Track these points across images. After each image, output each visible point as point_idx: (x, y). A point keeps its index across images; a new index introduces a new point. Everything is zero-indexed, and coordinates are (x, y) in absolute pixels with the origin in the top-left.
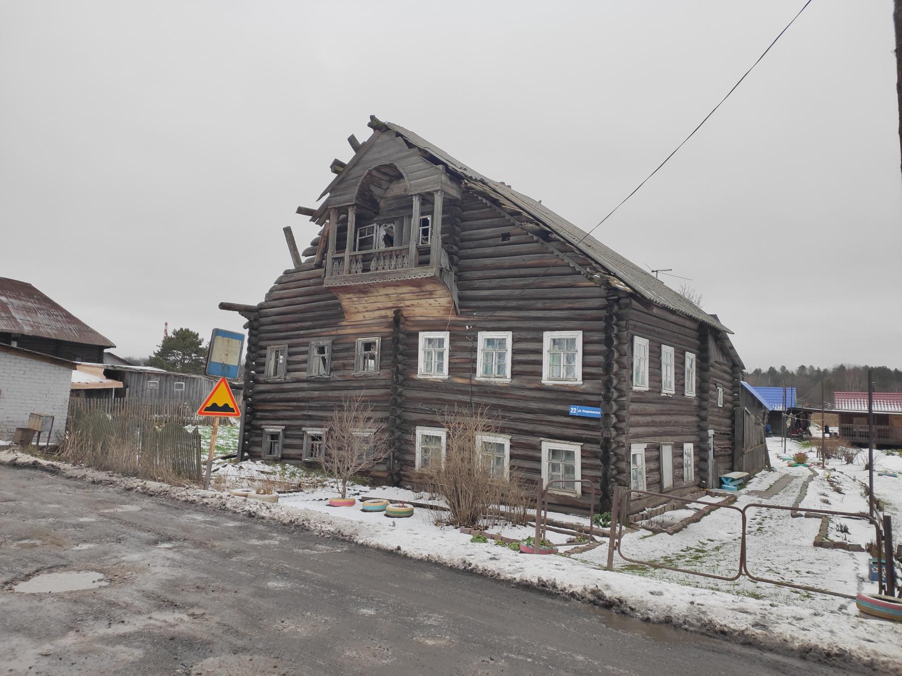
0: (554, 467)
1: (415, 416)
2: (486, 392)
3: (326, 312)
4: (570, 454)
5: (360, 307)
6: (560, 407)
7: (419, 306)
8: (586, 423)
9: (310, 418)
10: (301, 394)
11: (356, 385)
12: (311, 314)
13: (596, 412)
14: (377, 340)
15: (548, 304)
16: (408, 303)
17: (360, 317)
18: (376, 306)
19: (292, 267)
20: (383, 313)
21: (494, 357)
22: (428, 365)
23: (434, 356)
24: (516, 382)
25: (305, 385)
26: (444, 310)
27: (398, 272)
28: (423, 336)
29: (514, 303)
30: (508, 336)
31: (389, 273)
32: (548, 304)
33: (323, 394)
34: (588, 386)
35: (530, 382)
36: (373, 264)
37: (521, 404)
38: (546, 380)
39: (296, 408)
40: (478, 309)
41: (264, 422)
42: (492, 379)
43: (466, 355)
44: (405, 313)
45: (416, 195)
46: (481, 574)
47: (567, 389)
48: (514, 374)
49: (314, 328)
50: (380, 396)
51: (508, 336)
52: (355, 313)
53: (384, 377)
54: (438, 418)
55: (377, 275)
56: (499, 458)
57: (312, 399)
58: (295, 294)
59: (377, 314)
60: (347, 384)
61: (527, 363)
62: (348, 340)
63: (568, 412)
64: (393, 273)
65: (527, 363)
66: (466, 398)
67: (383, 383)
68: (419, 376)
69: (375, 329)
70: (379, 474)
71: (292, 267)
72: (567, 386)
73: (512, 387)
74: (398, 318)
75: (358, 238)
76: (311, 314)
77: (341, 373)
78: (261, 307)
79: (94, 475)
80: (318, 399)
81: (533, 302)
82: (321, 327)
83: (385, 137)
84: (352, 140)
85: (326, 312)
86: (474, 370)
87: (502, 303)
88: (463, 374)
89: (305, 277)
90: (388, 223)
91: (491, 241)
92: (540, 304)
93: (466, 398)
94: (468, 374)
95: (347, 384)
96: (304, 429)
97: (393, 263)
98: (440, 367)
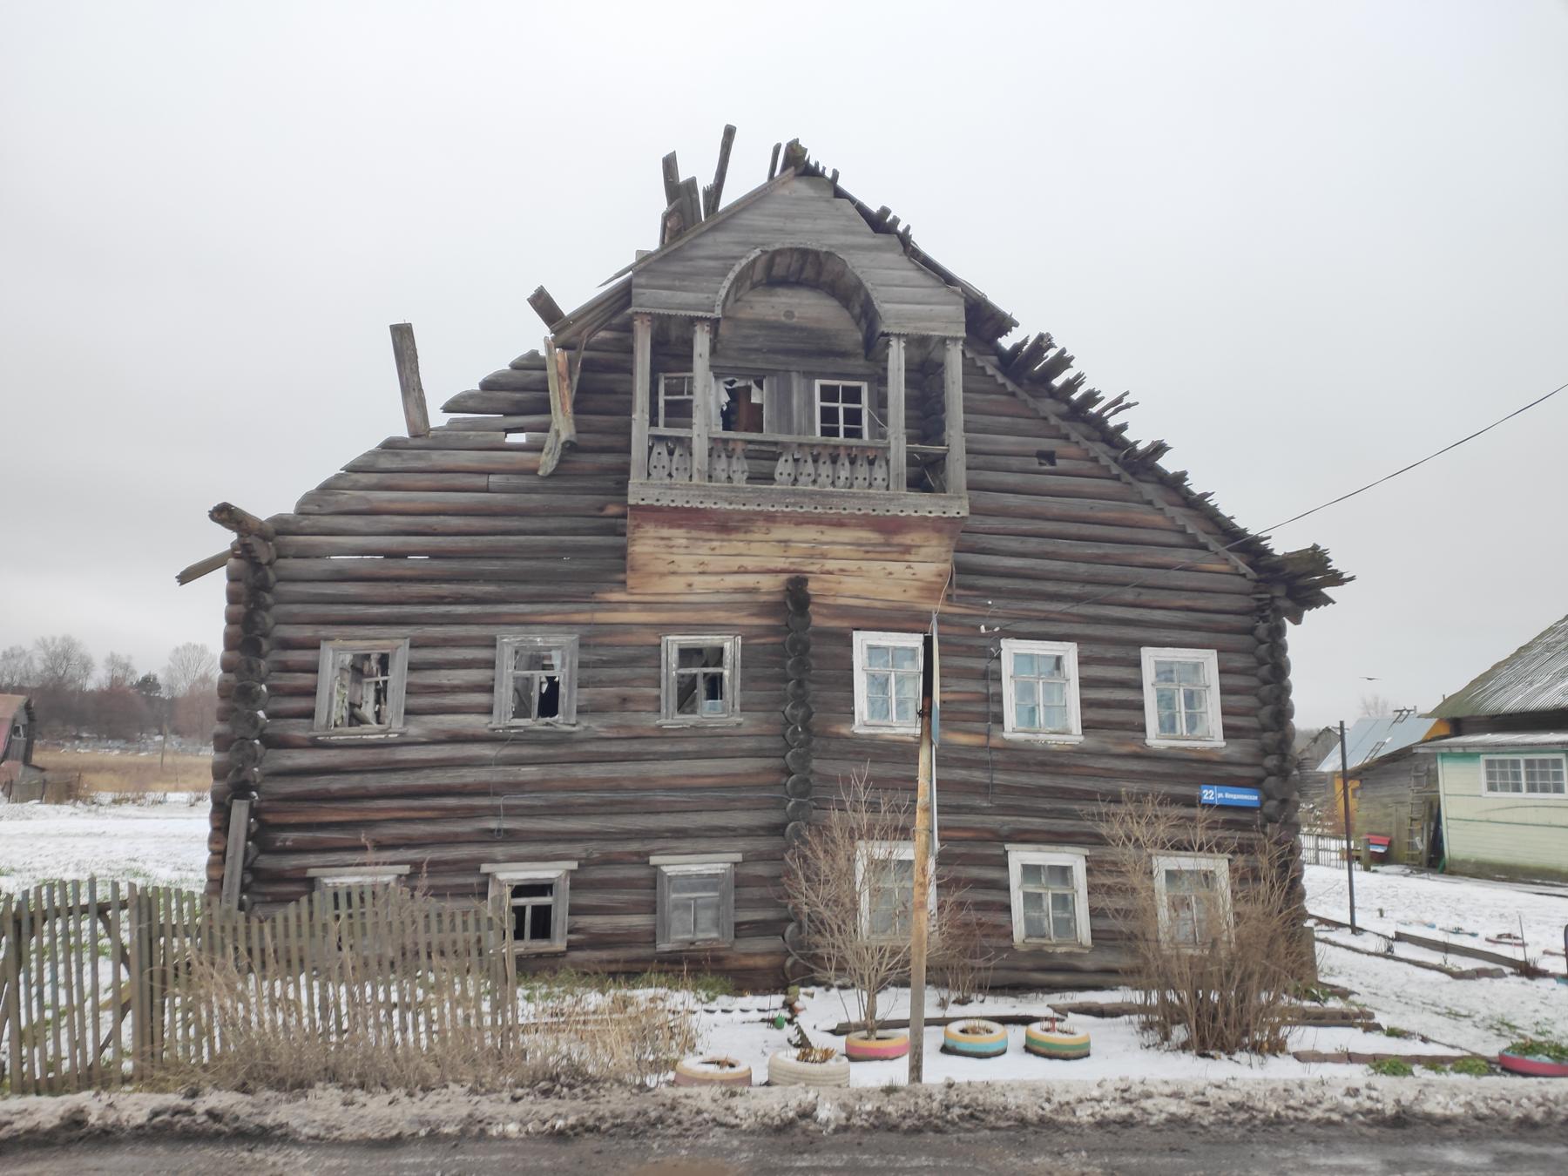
0: (1032, 900)
4: (1064, 873)
5: (685, 562)
6: (1181, 790)
7: (859, 573)
8: (1234, 818)
9: (510, 836)
10: (470, 776)
11: (666, 748)
12: (496, 565)
13: (1248, 797)
14: (731, 646)
15: (1147, 596)
16: (831, 565)
17: (676, 585)
18: (735, 563)
19: (402, 432)
20: (749, 581)
21: (1041, 693)
24: (1092, 742)
25: (487, 751)
26: (922, 589)
28: (862, 641)
29: (1075, 589)
30: (1069, 652)
32: (1147, 596)
33: (556, 772)
34: (1235, 750)
36: (783, 468)
40: (996, 593)
41: (311, 859)
42: (1041, 737)
43: (975, 686)
44: (813, 587)
45: (899, 336)
47: (1194, 755)
48: (1087, 726)
50: (748, 775)
51: (1069, 652)
52: (662, 575)
53: (752, 730)
55: (811, 495)
56: (1065, 897)
57: (517, 787)
58: (433, 506)
60: (636, 746)
61: (1113, 706)
65: (1113, 706)
66: (978, 776)
67: (749, 744)
68: (858, 728)
69: (721, 616)
70: (750, 962)
71: (402, 432)
72: (1194, 750)
73: (1079, 752)
74: (796, 596)
75: (662, 399)
76: (496, 565)
77: (615, 718)
78: (281, 527)
81: (1116, 589)
83: (802, 188)
86: (999, 719)
87: (1050, 587)
88: (969, 725)
90: (742, 377)
91: (1015, 462)
92: (1129, 595)
93: (978, 776)
95: (636, 746)
96: (485, 868)
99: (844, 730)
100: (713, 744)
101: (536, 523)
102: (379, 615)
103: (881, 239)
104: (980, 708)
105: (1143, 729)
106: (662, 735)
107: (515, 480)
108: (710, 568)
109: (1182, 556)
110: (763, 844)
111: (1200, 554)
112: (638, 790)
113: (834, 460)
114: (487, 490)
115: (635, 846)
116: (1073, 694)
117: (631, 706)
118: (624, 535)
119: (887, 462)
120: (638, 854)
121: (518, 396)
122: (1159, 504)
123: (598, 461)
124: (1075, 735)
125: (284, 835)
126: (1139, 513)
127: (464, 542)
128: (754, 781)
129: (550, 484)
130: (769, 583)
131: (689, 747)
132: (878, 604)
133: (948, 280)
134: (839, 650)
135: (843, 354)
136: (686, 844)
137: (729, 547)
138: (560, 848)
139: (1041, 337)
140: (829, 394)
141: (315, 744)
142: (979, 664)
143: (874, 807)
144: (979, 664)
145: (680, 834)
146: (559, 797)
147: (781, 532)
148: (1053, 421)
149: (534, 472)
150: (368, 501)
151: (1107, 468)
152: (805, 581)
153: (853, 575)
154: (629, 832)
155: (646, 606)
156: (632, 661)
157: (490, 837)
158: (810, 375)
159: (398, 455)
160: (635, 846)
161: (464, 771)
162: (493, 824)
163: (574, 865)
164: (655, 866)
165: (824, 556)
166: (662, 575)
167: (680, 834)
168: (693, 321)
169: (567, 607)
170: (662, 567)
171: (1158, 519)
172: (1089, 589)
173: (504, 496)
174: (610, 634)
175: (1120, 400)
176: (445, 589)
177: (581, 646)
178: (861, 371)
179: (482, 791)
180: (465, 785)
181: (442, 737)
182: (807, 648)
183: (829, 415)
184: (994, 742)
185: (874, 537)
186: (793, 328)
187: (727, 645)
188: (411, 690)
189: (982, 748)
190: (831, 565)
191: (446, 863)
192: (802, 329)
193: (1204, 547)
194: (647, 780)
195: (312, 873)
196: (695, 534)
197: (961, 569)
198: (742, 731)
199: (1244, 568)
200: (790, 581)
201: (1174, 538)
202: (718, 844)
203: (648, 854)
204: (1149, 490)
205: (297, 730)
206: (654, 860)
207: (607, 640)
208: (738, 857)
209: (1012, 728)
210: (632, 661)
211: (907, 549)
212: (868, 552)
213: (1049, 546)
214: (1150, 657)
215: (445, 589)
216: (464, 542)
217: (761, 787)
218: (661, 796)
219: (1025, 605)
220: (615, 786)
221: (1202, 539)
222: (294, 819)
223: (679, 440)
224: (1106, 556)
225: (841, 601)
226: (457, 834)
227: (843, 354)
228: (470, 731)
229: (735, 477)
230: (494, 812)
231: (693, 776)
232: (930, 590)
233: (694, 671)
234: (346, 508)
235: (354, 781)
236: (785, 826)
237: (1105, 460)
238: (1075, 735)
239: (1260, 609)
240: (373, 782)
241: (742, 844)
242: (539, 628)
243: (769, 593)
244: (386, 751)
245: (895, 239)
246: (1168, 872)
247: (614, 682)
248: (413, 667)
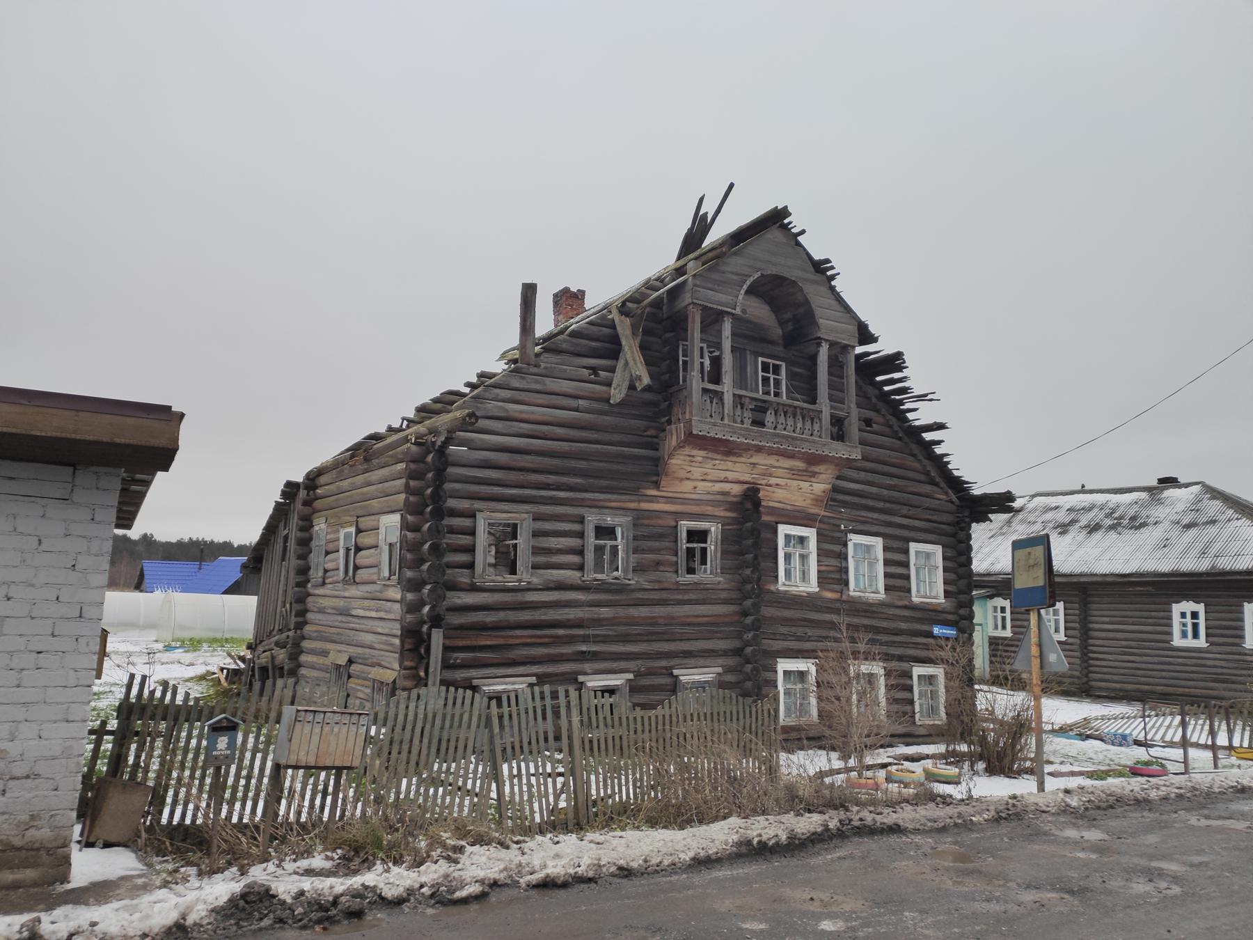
1: (778, 645)
2: (858, 611)
3: (615, 467)
5: (697, 472)
6: (925, 628)
7: (785, 487)
9: (595, 656)
12: (583, 465)
14: (714, 529)
16: (773, 481)
18: (723, 475)
22: (788, 574)
23: (796, 561)
27: (814, 442)
28: (783, 530)
29: (880, 505)
31: (802, 439)
33: (621, 612)
35: (901, 598)
37: (892, 625)
38: (916, 599)
39: (558, 641)
41: (473, 673)
46: (788, 845)
48: (888, 588)
49: (586, 491)
50: (726, 616)
53: (726, 586)
54: (930, 654)
55: (784, 436)
57: (598, 622)
59: (719, 487)
60: (664, 595)
62: (660, 522)
63: (932, 633)
64: (807, 440)
67: (724, 595)
69: (709, 510)
73: (882, 604)
76: (583, 465)
77: (653, 576)
79: (203, 894)
80: (612, 622)
82: (602, 490)
84: (803, 232)
85: (615, 467)
86: (846, 583)
87: (870, 503)
89: (570, 391)
92: (905, 510)
94: (837, 587)
95: (664, 595)
97: (799, 425)
98: (804, 576)
99: (772, 588)
100: (704, 595)
101: (607, 437)
102: (512, 495)
103: (818, 277)
104: (837, 576)
105: (909, 591)
106: (678, 588)
107: (595, 405)
108: (709, 477)
109: (927, 489)
110: (731, 661)
111: (935, 488)
112: (666, 625)
113: (794, 416)
114: (577, 410)
115: (663, 663)
116: (880, 569)
117: (662, 568)
118: (657, 450)
119: (820, 420)
120: (666, 668)
121: (594, 344)
122: (920, 457)
123: (661, 400)
124: (882, 596)
125: (456, 655)
126: (910, 462)
127: (565, 446)
128: (727, 620)
129: (616, 410)
130: (736, 489)
131: (693, 596)
132: (789, 507)
133: (847, 309)
134: (769, 536)
135: (772, 343)
136: (692, 661)
137: (723, 465)
138: (622, 664)
139: (898, 355)
140: (765, 368)
141: (474, 588)
142: (837, 548)
143: (853, 640)
144: (837, 548)
145: (688, 654)
146: (622, 629)
147: (759, 459)
148: (874, 400)
149: (607, 400)
150: (507, 411)
151: (896, 432)
152: (758, 490)
153: (790, 489)
154: (661, 653)
155: (669, 500)
156: (660, 537)
157: (582, 657)
158: (757, 354)
159: (523, 378)
160: (663, 663)
161: (567, 610)
162: (584, 648)
163: (631, 676)
164: (677, 677)
165: (770, 475)
166: (682, 480)
167: (688, 654)
168: (722, 314)
169: (623, 497)
170: (682, 474)
171: (917, 465)
172: (888, 505)
173: (587, 416)
174: (649, 518)
175: (926, 395)
176: (552, 479)
177: (634, 525)
178: (782, 355)
179: (579, 624)
180: (569, 620)
181: (552, 585)
182: (759, 534)
183: (766, 381)
184: (844, 597)
185: (799, 464)
186: (747, 321)
187: (713, 529)
188: (537, 551)
189: (837, 600)
190: (773, 481)
191: (556, 675)
192: (751, 322)
193: (937, 485)
194: (673, 618)
195: (475, 682)
196: (710, 455)
197: (835, 489)
198: (720, 587)
199: (954, 498)
200: (748, 489)
201: (922, 478)
202: (708, 661)
203: (672, 668)
204: (915, 448)
205: (463, 577)
206: (676, 672)
207: (646, 522)
208: (720, 670)
209: (853, 590)
210: (660, 537)
211: (814, 474)
212: (795, 474)
213: (870, 477)
214: (914, 547)
215: (552, 479)
216: (565, 446)
217: (727, 624)
218: (678, 629)
219: (858, 513)
220: (652, 622)
221: (938, 479)
222: (461, 643)
223: (716, 392)
224: (895, 486)
225: (771, 504)
226: (562, 654)
227: (772, 343)
228: (570, 582)
229: (746, 420)
230: (585, 639)
231: (698, 616)
232: (817, 501)
233: (695, 545)
234: (491, 414)
235: (501, 616)
236: (742, 649)
237: (896, 428)
238: (882, 596)
239: (958, 523)
240: (513, 616)
241: (720, 661)
242: (607, 511)
243: (735, 496)
244: (519, 594)
245: (824, 278)
246: (785, 672)
247: (651, 551)
248: (536, 534)
